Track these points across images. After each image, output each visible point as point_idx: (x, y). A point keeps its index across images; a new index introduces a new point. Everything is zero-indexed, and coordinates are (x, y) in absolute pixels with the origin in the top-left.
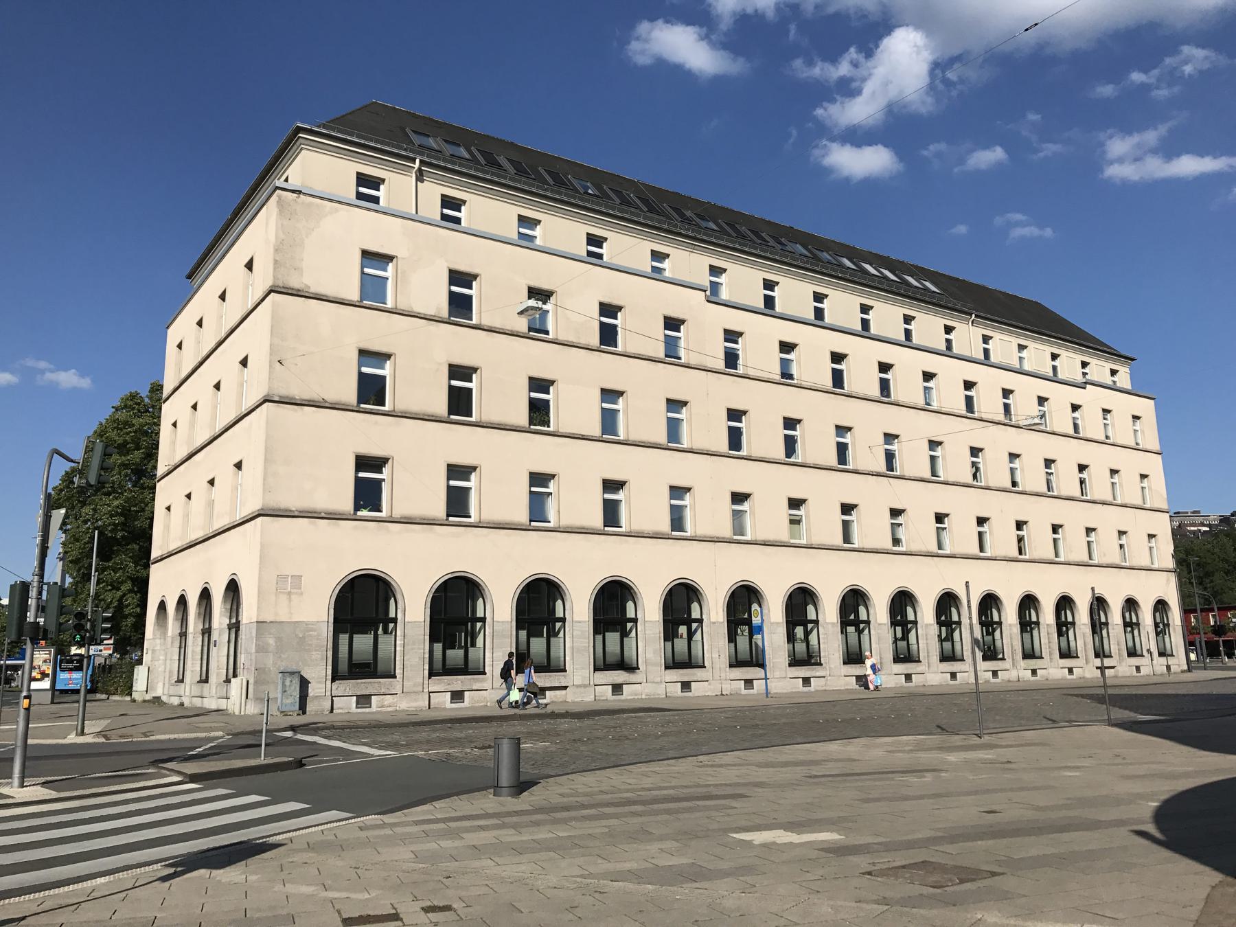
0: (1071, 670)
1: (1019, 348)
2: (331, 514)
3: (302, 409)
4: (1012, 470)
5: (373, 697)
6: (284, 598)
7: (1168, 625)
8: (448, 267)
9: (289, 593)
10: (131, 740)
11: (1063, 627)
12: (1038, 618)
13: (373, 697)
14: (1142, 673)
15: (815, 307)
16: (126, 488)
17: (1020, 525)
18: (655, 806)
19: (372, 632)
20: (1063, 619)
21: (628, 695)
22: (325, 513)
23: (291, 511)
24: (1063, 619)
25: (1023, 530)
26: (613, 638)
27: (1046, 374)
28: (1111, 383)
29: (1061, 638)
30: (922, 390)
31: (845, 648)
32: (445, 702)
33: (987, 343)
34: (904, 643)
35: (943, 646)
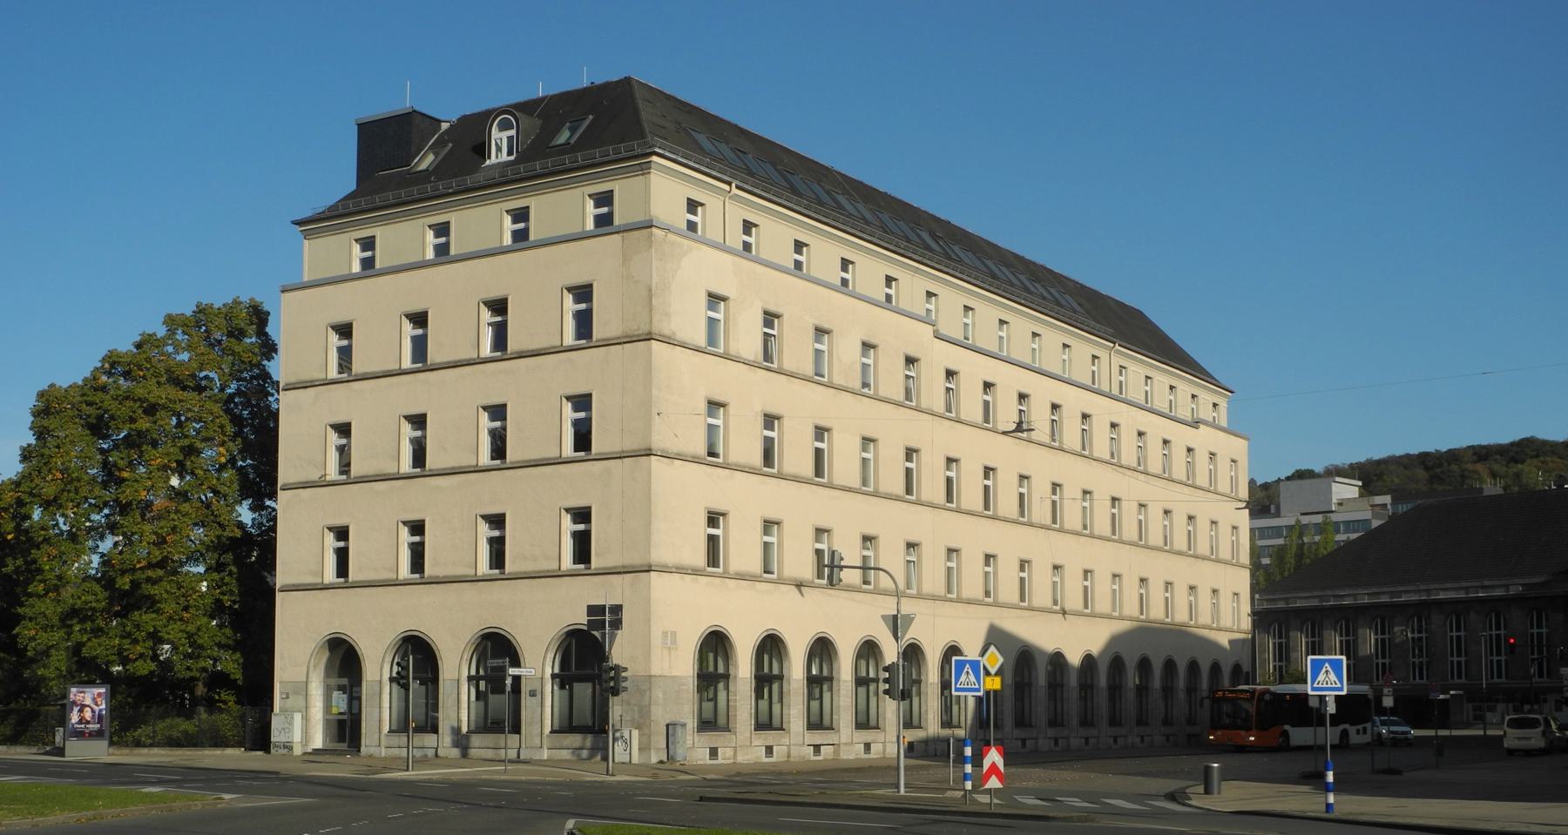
0: (817, 748)
1: (927, 296)
2: (754, 576)
3: (673, 463)
4: (712, 429)
5: (822, 747)
6: (666, 652)
7: (918, 682)
8: (707, 291)
9: (669, 649)
10: (1481, 733)
11: (818, 683)
12: (781, 668)
13: (822, 747)
14: (720, 761)
15: (688, 221)
16: (37, 481)
17: (713, 519)
18: (1262, 800)
19: (567, 687)
20: (711, 669)
21: (875, 754)
22: (692, 570)
23: (668, 567)
24: (711, 669)
25: (718, 527)
26: (583, 691)
27: (1135, 400)
28: (924, 313)
29: (759, 701)
30: (943, 391)
31: (566, 711)
32: (809, 755)
33: (695, 214)
34: (711, 704)
35: (703, 706)
